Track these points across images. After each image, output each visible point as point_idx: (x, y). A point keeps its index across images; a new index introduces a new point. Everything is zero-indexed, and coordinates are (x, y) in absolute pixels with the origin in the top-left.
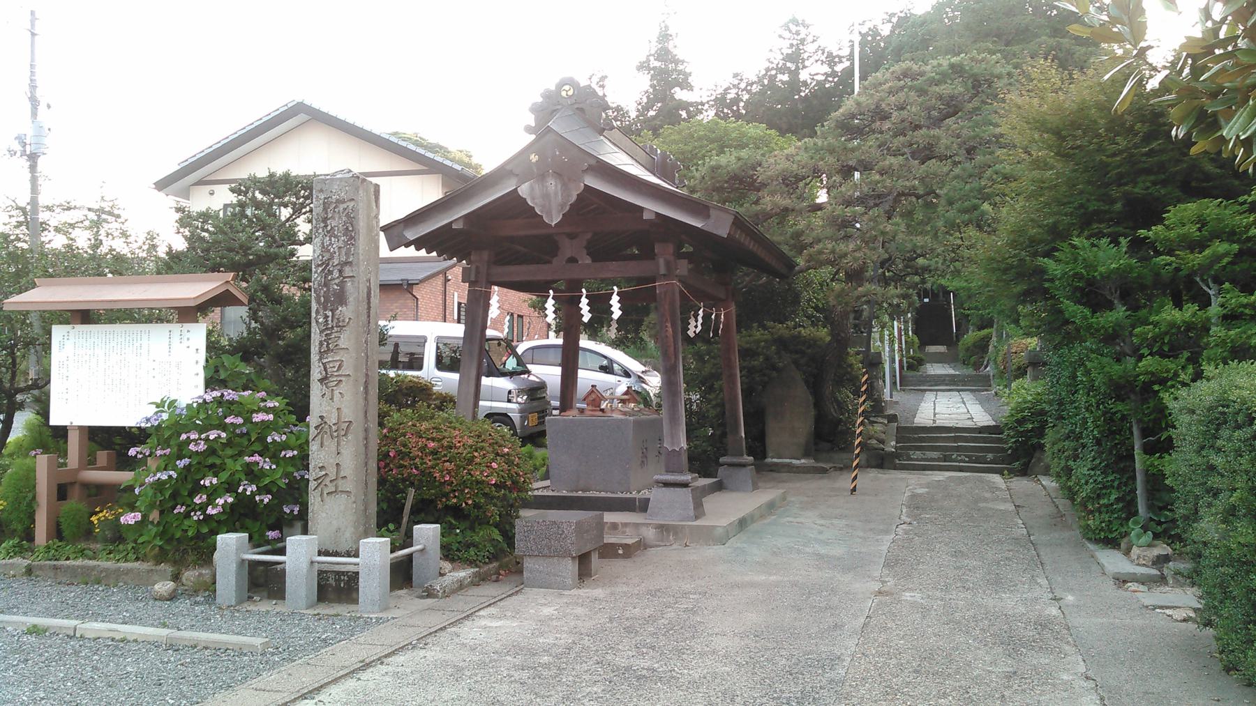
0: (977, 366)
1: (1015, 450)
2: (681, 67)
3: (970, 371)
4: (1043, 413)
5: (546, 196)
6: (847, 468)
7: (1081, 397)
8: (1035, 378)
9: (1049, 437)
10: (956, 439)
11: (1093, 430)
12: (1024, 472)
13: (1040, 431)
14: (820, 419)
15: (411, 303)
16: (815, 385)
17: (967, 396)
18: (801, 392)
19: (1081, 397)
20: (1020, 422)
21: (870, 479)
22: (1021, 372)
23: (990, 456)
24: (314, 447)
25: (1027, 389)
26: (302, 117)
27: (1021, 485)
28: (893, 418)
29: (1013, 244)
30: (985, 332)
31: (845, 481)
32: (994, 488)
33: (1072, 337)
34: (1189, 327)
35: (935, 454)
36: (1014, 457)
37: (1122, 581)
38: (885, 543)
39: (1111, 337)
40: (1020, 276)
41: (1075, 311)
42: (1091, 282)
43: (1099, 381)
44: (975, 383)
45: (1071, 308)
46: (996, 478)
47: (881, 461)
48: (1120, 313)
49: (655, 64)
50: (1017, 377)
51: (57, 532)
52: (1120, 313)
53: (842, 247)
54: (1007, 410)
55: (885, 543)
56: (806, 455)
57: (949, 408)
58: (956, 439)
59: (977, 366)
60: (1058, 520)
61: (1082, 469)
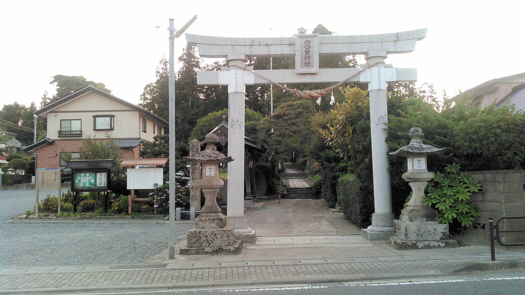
0: (303, 170)
1: (315, 193)
2: (196, 60)
3: (300, 172)
4: (321, 184)
5: (222, 140)
6: (277, 198)
7: (327, 180)
8: (320, 175)
9: (323, 188)
10: (301, 191)
11: (329, 186)
12: (317, 198)
13: (321, 188)
14: (269, 186)
15: (132, 154)
16: (267, 179)
17: (302, 180)
18: (264, 180)
19: (327, 180)
20: (316, 186)
21: (282, 200)
22: (316, 173)
23: (309, 195)
24: (191, 192)
25: (318, 178)
26: (90, 91)
27: (316, 201)
28: (285, 186)
29: (314, 148)
30: (306, 158)
31: (278, 201)
32: (310, 201)
33: (325, 168)
34: (345, 167)
35: (296, 195)
36: (314, 195)
37: (334, 212)
38: (291, 210)
39: (332, 168)
40: (316, 155)
41: (326, 163)
42: (329, 158)
43: (330, 176)
44: (303, 176)
45: (325, 163)
46: (311, 200)
47: (284, 197)
48: (334, 164)
49: (185, 57)
50: (315, 174)
51: (133, 210)
52: (334, 164)
53: (278, 147)
54: (313, 183)
55: (291, 210)
56: (266, 195)
57: (296, 183)
58: (301, 191)
59: (303, 170)
60: (324, 205)
61: (328, 194)
